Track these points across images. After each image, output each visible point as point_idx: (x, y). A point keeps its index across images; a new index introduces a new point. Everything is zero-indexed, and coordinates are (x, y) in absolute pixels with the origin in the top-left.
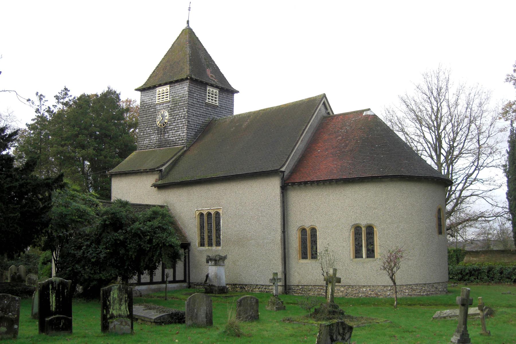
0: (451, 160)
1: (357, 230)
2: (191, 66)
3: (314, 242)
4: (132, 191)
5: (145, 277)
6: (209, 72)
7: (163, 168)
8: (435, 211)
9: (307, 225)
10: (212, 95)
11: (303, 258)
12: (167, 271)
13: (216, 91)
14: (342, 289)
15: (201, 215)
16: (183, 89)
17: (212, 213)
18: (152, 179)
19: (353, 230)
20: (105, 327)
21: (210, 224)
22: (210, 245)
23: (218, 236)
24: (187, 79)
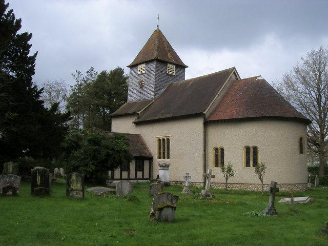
1: (248, 149)
2: (159, 54)
3: (223, 157)
4: (122, 126)
6: (169, 55)
7: (139, 112)
8: (297, 140)
9: (219, 146)
10: (171, 69)
11: (247, 166)
12: (138, 172)
13: (173, 67)
16: (153, 66)
19: (245, 150)
22: (164, 158)
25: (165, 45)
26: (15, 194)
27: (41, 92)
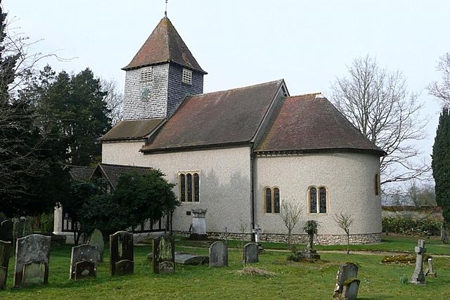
0: (374, 132)
1: (312, 190)
3: (277, 200)
4: (116, 155)
5: (138, 228)
7: (149, 136)
9: (272, 186)
10: (187, 76)
11: (268, 212)
13: (190, 73)
14: (300, 237)
15: (182, 175)
17: (192, 174)
18: (140, 145)
19: (309, 190)
20: (156, 271)
21: (189, 183)
22: (190, 200)
23: (197, 193)
24: (167, 62)
25: (177, 39)
26: (92, 274)
27: (106, 93)
